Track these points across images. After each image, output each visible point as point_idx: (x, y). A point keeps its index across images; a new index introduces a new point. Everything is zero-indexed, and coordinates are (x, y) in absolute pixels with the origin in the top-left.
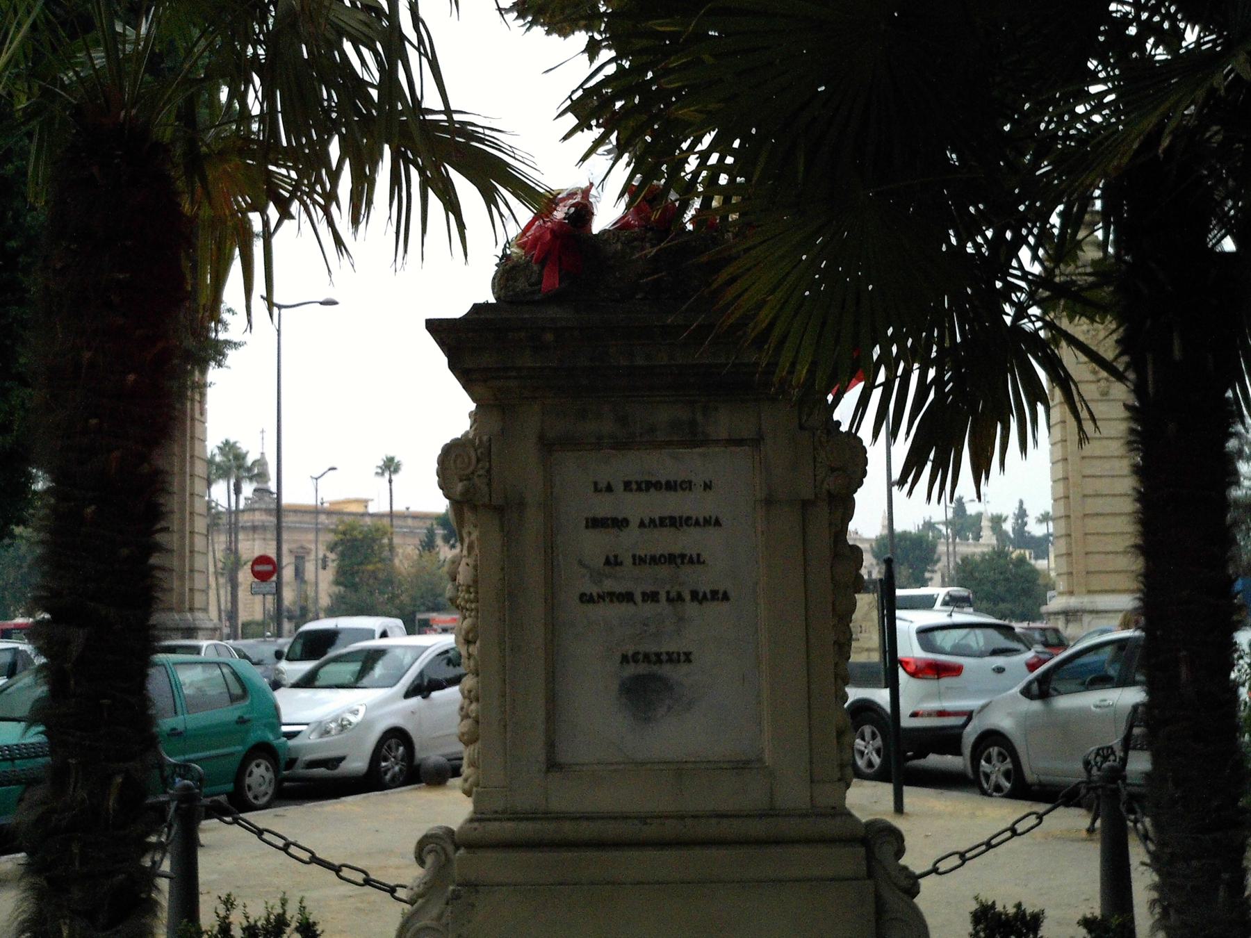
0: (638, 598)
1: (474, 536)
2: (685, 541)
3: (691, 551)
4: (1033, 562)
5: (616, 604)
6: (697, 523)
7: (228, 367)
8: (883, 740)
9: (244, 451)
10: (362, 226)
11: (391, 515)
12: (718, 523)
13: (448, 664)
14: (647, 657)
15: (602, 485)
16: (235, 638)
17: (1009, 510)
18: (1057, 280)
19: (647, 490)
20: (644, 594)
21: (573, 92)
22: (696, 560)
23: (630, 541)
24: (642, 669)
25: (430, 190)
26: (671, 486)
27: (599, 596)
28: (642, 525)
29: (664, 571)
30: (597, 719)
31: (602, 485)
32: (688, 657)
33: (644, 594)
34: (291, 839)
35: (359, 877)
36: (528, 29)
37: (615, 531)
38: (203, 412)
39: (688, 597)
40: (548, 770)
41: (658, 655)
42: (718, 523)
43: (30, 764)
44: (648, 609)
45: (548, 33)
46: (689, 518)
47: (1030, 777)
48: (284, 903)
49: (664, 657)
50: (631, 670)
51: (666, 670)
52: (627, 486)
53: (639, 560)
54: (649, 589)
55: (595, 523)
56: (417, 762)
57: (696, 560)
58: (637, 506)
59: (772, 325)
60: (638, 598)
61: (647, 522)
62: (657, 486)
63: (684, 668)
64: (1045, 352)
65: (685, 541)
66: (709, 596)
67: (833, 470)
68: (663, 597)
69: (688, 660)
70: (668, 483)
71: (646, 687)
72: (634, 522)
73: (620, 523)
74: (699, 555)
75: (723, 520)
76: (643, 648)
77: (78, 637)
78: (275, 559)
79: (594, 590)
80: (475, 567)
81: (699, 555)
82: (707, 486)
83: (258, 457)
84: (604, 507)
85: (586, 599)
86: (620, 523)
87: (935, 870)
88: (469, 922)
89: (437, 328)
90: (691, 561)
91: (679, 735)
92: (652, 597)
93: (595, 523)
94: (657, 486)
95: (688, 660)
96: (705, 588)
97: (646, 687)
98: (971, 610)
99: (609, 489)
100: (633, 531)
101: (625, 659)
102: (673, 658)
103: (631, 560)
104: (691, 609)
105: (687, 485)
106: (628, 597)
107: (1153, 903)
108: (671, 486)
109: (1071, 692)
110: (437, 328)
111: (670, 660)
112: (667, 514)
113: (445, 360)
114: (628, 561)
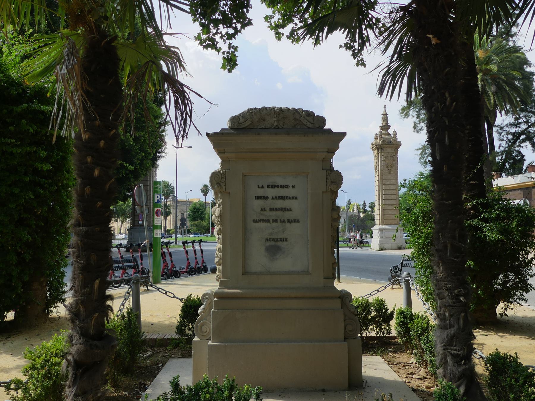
0: (271, 221)
1: (221, 201)
2: (286, 204)
5: (280, 207)
6: (290, 198)
8: (470, 350)
10: (185, 139)
11: (205, 203)
13: (286, 239)
14: (274, 240)
15: (260, 186)
16: (80, 226)
17: (361, 203)
18: (502, 119)
19: (274, 188)
20: (273, 220)
22: (290, 210)
23: (269, 203)
24: (273, 243)
25: (167, 72)
26: (282, 187)
28: (273, 198)
29: (279, 213)
30: (259, 259)
31: (260, 186)
32: (286, 240)
33: (273, 220)
34: (167, 290)
35: (172, 295)
36: (184, 69)
37: (265, 200)
38: (156, 174)
39: (287, 222)
41: (277, 239)
42: (296, 198)
43: (488, 104)
44: (274, 224)
45: (346, 49)
46: (287, 197)
48: (394, 309)
49: (279, 240)
50: (269, 243)
51: (279, 243)
52: (268, 187)
53: (271, 210)
54: (274, 218)
55: (258, 198)
57: (290, 210)
58: (271, 193)
60: (271, 221)
62: (278, 186)
63: (285, 243)
65: (286, 204)
67: (332, 182)
68: (279, 221)
69: (286, 241)
70: (281, 186)
71: (274, 247)
72: (270, 197)
73: (266, 198)
75: (298, 197)
76: (272, 237)
77: (242, 120)
79: (258, 219)
80: (221, 211)
82: (293, 187)
83: (365, 54)
84: (261, 192)
85: (255, 221)
86: (266, 198)
87: (174, 297)
89: (344, 135)
90: (288, 210)
91: (283, 263)
92: (275, 221)
93: (258, 198)
94: (278, 186)
95: (286, 241)
96: (292, 218)
97: (274, 247)
98: (332, 160)
99: (263, 187)
100: (269, 201)
101: (267, 240)
102: (282, 240)
104: (288, 225)
105: (287, 187)
106: (268, 221)
107: (122, 78)
108: (282, 187)
110: (344, 135)
111: (281, 241)
112: (280, 195)
113: (268, 106)
114: (268, 210)
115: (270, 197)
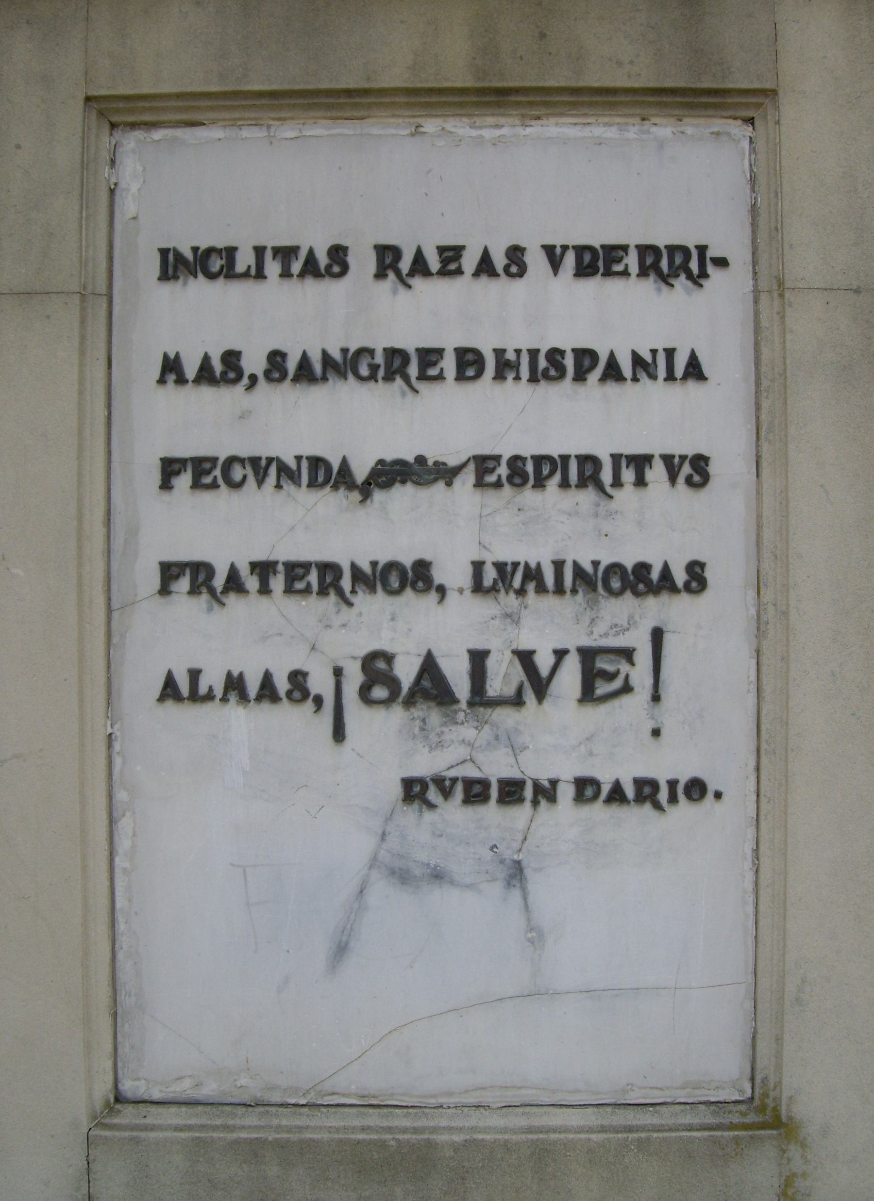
4: (130, 198)
7: (338, 612)
9: (159, 462)
12: (695, 370)
19: (540, 483)
21: (124, 763)
27: (637, 361)
40: (162, 698)
47: (367, 354)
53: (418, 577)
56: (173, 372)
59: (243, 1128)
64: (429, 472)
66: (434, 262)
74: (195, 675)
78: (544, 682)
81: (195, 675)
88: (557, 542)
103: (528, 259)
109: (171, 127)
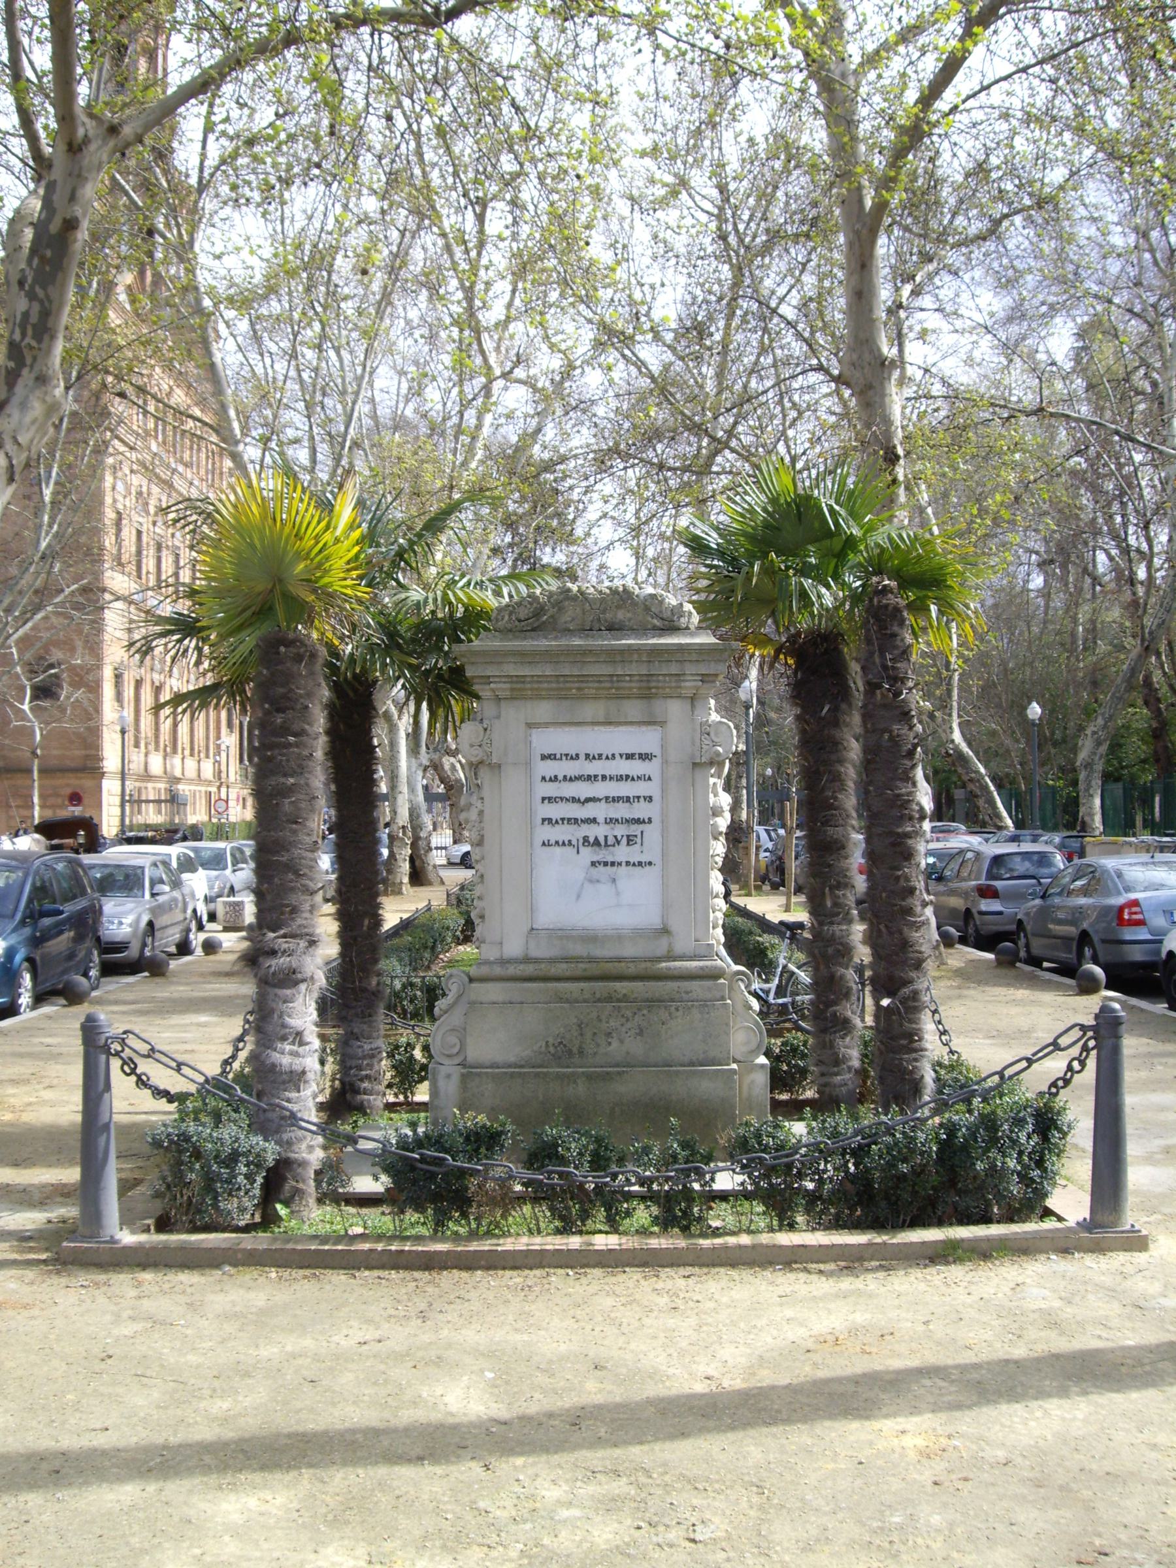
3: (547, 827)
53: (594, 821)
61: (592, 840)
115: (601, 820)
